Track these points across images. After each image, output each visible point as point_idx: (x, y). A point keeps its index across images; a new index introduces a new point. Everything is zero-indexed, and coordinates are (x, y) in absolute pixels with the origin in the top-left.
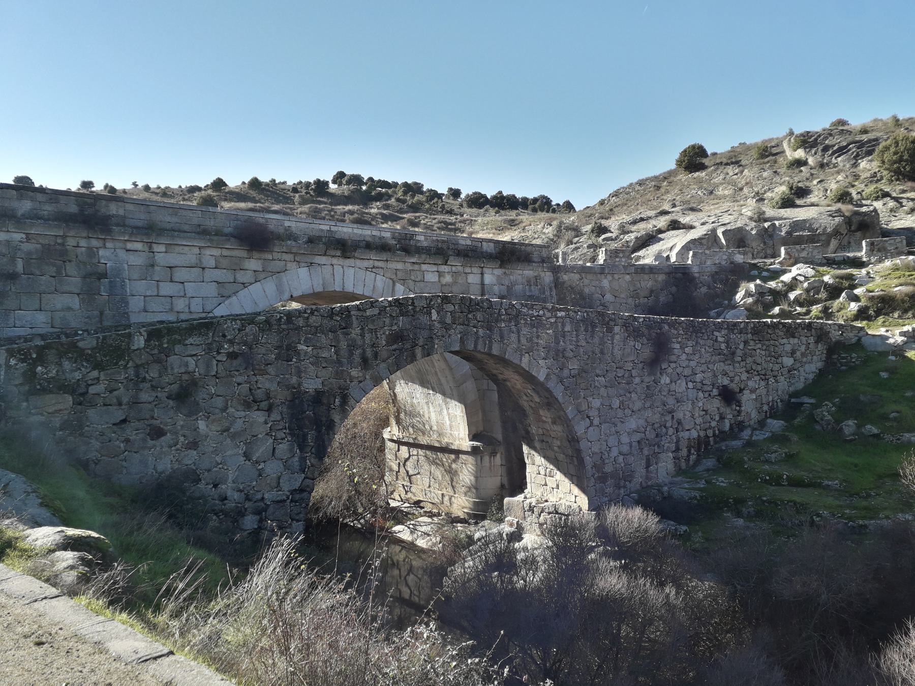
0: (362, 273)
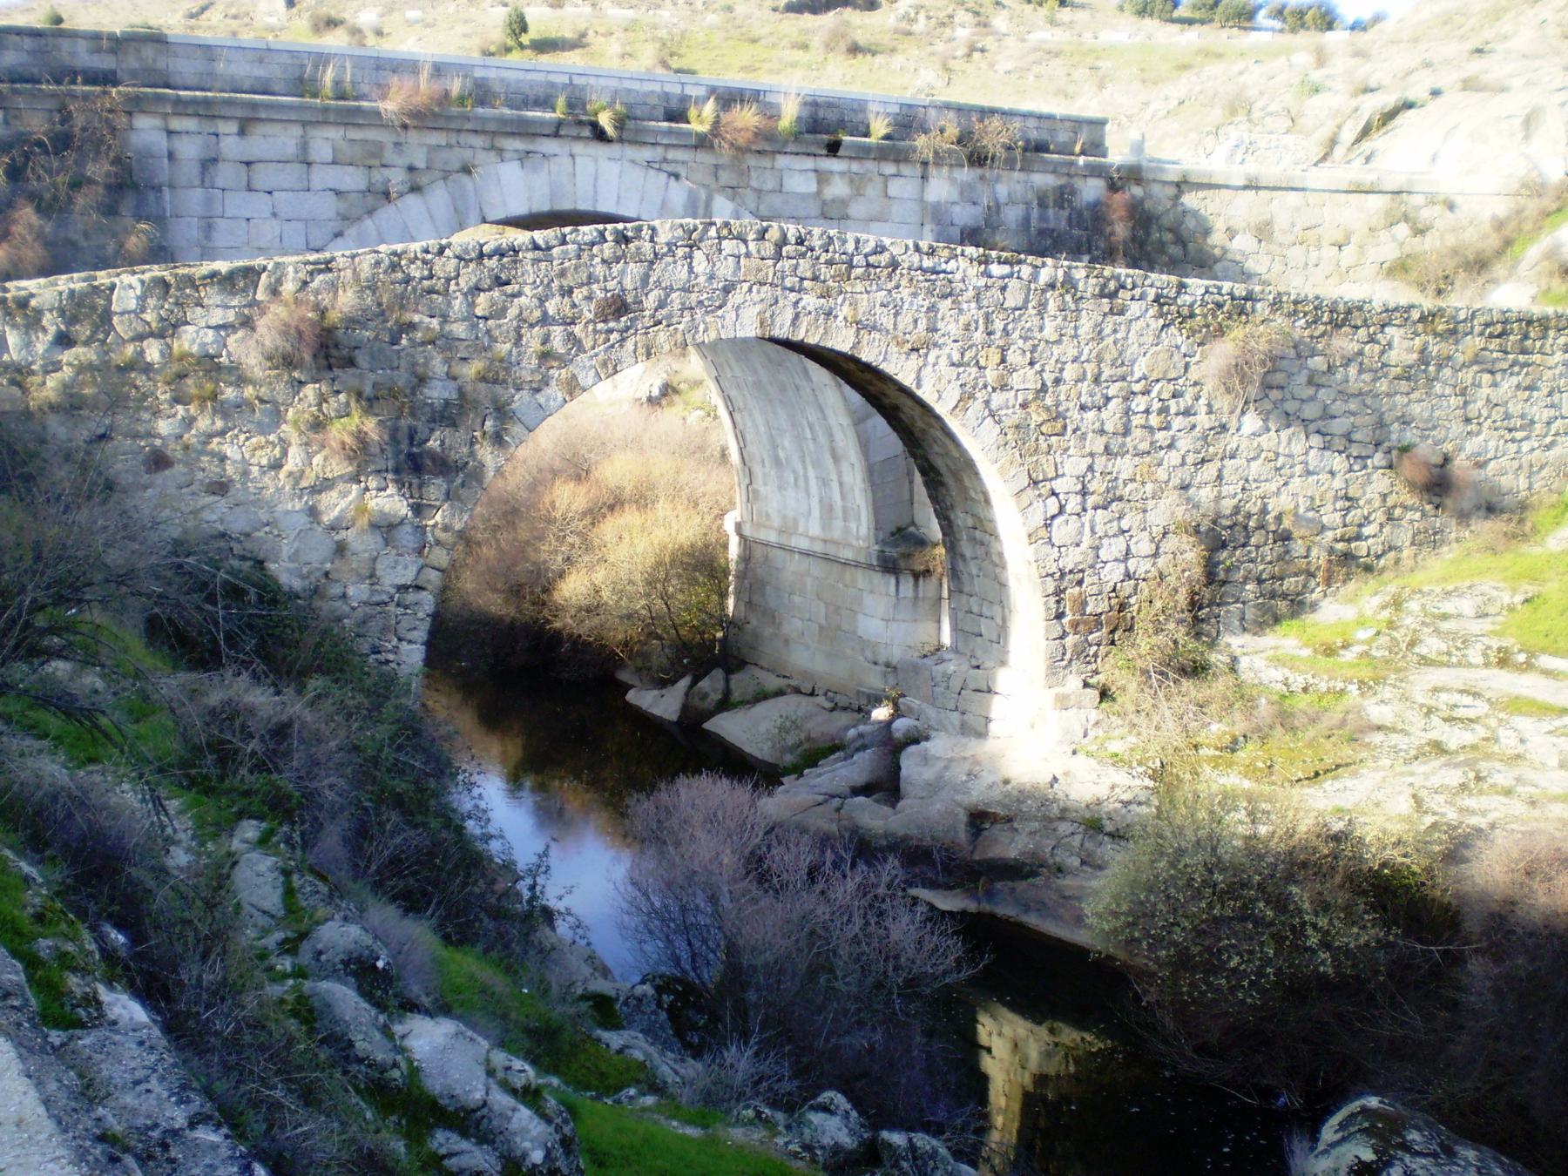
0: (637, 174)
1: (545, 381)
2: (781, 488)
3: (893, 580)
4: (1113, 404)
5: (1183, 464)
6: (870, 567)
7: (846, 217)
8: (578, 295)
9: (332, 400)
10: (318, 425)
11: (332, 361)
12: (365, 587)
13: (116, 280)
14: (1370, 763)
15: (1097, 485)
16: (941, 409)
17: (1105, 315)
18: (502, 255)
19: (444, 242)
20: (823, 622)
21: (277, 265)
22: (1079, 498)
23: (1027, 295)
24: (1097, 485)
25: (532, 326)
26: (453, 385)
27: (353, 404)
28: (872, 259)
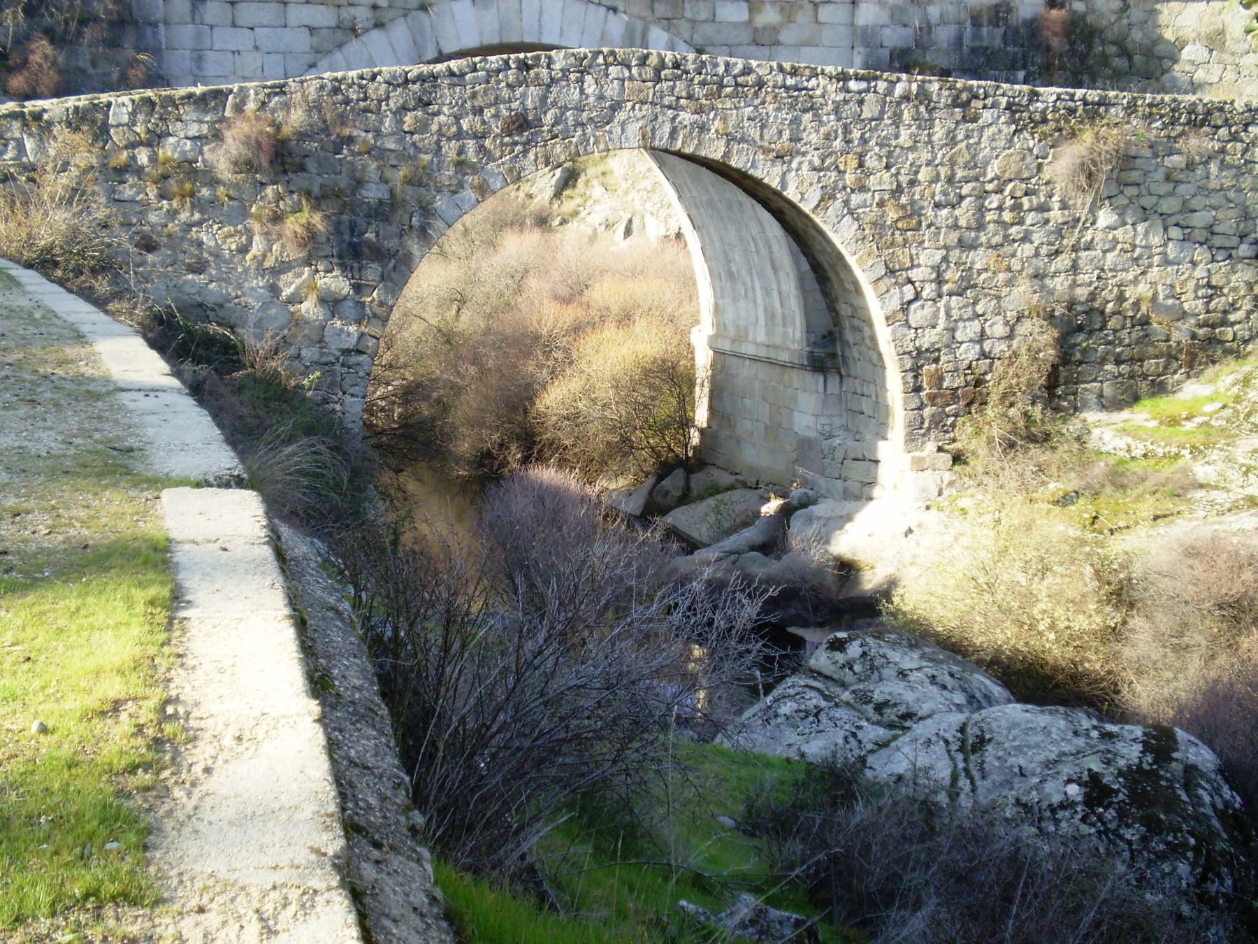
1: (461, 185)
2: (735, 300)
3: (821, 379)
4: (965, 203)
5: (1037, 255)
6: (802, 367)
7: (777, 43)
8: (488, 113)
9: (287, 199)
10: (277, 218)
11: (287, 167)
12: (315, 349)
13: (112, 99)
14: (1186, 515)
15: (952, 275)
16: (806, 208)
17: (957, 123)
18: (424, 81)
19: (376, 70)
20: (768, 422)
21: (241, 89)
22: (934, 286)
23: (883, 107)
24: (952, 275)
25: (449, 139)
26: (384, 188)
27: (304, 202)
28: (740, 80)
